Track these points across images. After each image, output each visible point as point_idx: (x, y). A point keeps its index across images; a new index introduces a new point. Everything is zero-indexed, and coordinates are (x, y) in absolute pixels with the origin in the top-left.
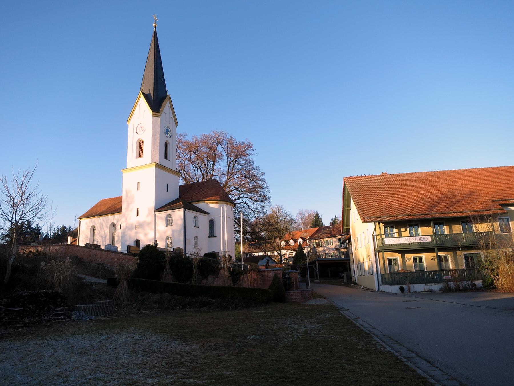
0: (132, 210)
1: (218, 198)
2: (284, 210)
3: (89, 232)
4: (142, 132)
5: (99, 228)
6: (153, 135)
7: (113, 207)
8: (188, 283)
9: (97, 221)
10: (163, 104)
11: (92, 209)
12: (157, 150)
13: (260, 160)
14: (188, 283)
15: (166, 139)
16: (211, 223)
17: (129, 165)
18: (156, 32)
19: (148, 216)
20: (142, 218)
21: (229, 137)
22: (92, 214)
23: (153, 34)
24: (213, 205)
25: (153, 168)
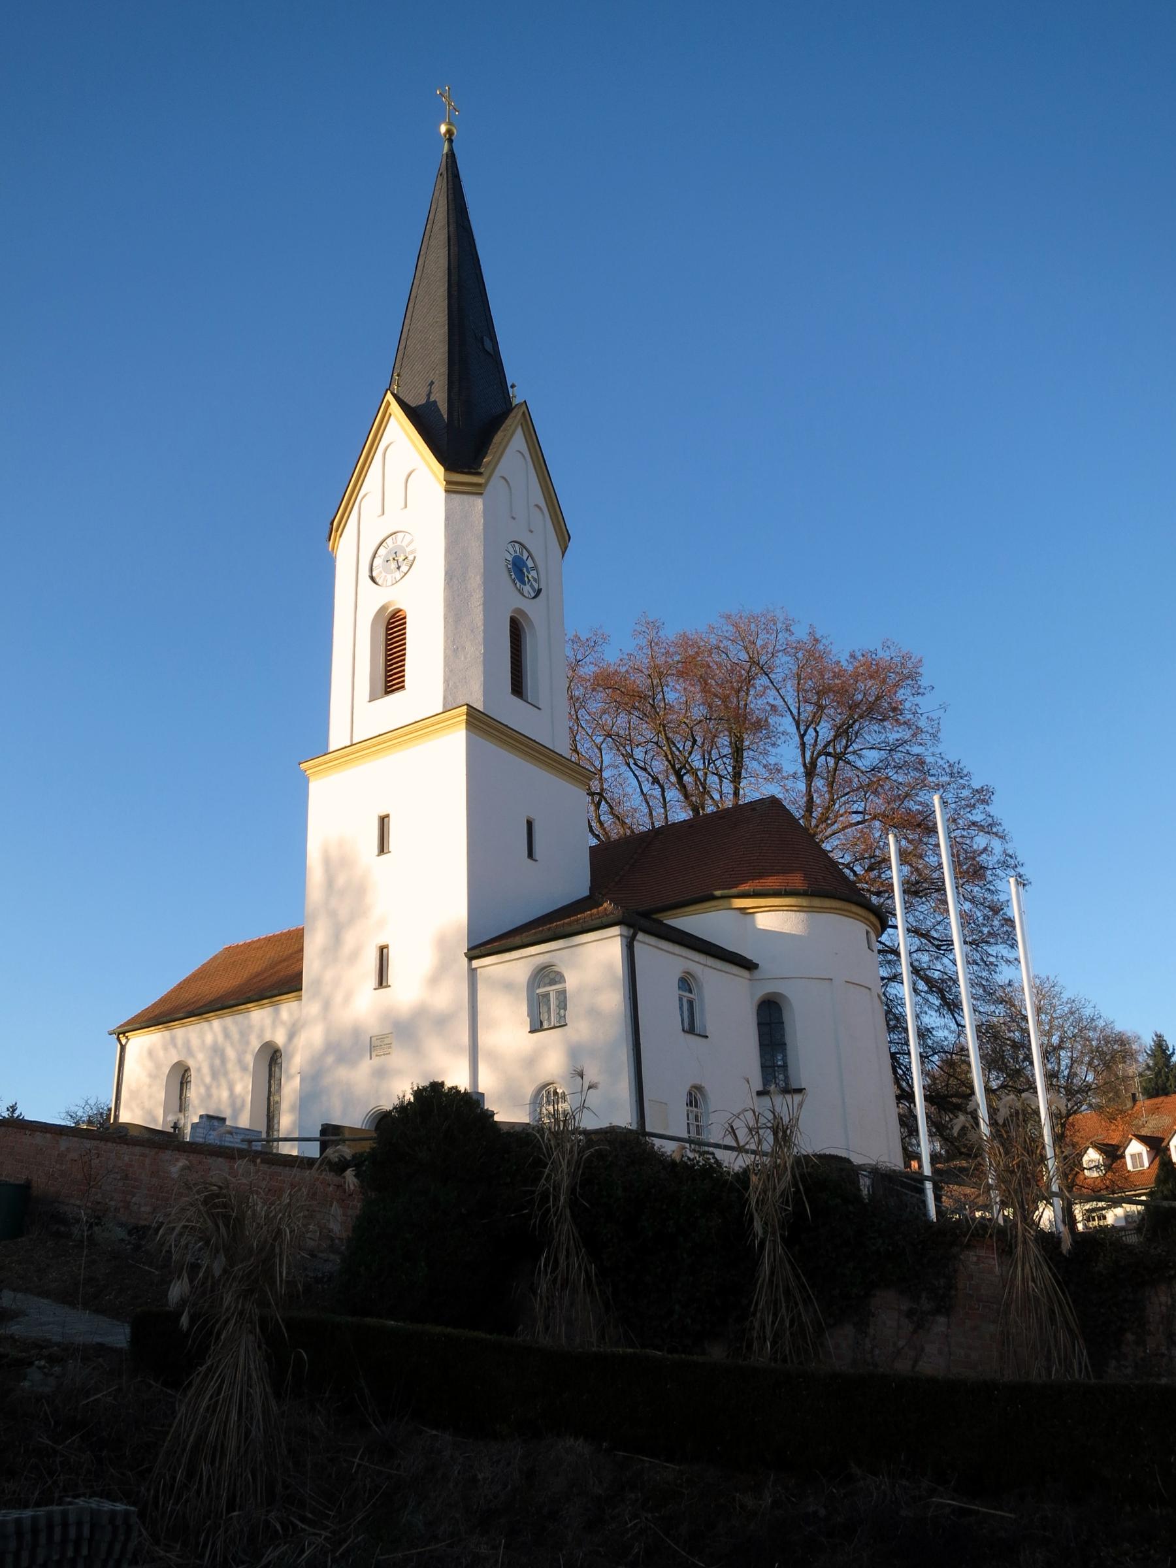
0: (354, 956)
1: (797, 880)
2: (1065, 996)
3: (162, 1096)
4: (398, 575)
5: (206, 1070)
6: (450, 576)
7: (270, 974)
8: (717, 1353)
9: (200, 1037)
10: (497, 438)
11: (180, 987)
12: (474, 650)
13: (965, 726)
14: (717, 1353)
15: (512, 600)
16: (771, 1016)
17: (338, 737)
18: (451, 155)
19: (434, 980)
20: (409, 987)
21: (801, 633)
22: (176, 1009)
23: (437, 162)
24: (775, 919)
25: (454, 742)
